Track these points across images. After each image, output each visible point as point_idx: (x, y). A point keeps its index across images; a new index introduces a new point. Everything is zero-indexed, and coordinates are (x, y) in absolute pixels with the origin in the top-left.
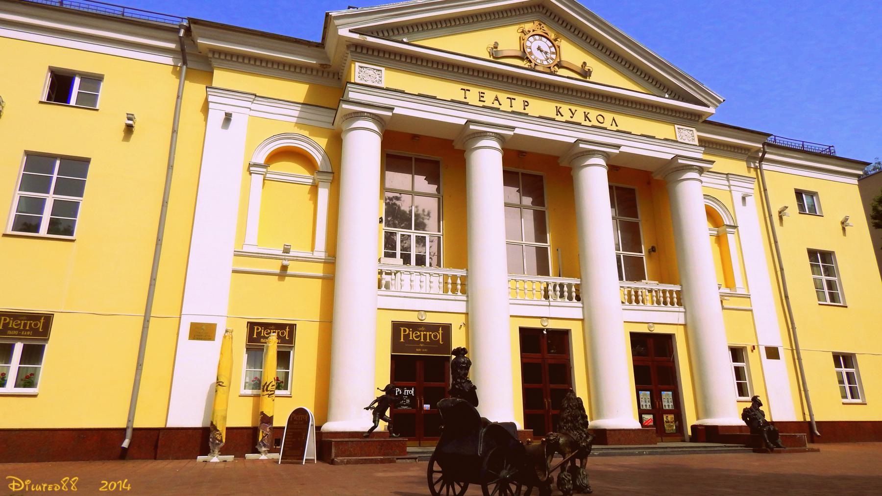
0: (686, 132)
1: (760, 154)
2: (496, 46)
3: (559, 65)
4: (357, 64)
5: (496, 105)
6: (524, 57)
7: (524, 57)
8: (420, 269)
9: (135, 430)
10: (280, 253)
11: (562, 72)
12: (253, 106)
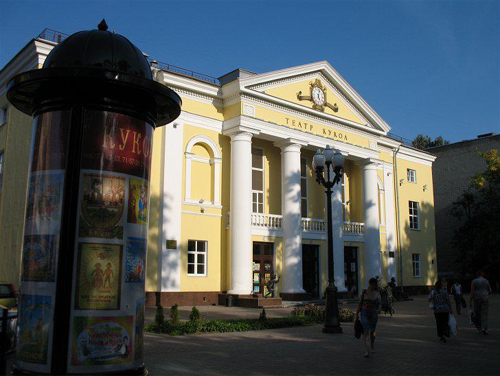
1: (397, 150)
2: (300, 93)
5: (299, 128)
6: (311, 99)
7: (311, 99)
8: (261, 214)
10: (198, 202)
11: (327, 109)
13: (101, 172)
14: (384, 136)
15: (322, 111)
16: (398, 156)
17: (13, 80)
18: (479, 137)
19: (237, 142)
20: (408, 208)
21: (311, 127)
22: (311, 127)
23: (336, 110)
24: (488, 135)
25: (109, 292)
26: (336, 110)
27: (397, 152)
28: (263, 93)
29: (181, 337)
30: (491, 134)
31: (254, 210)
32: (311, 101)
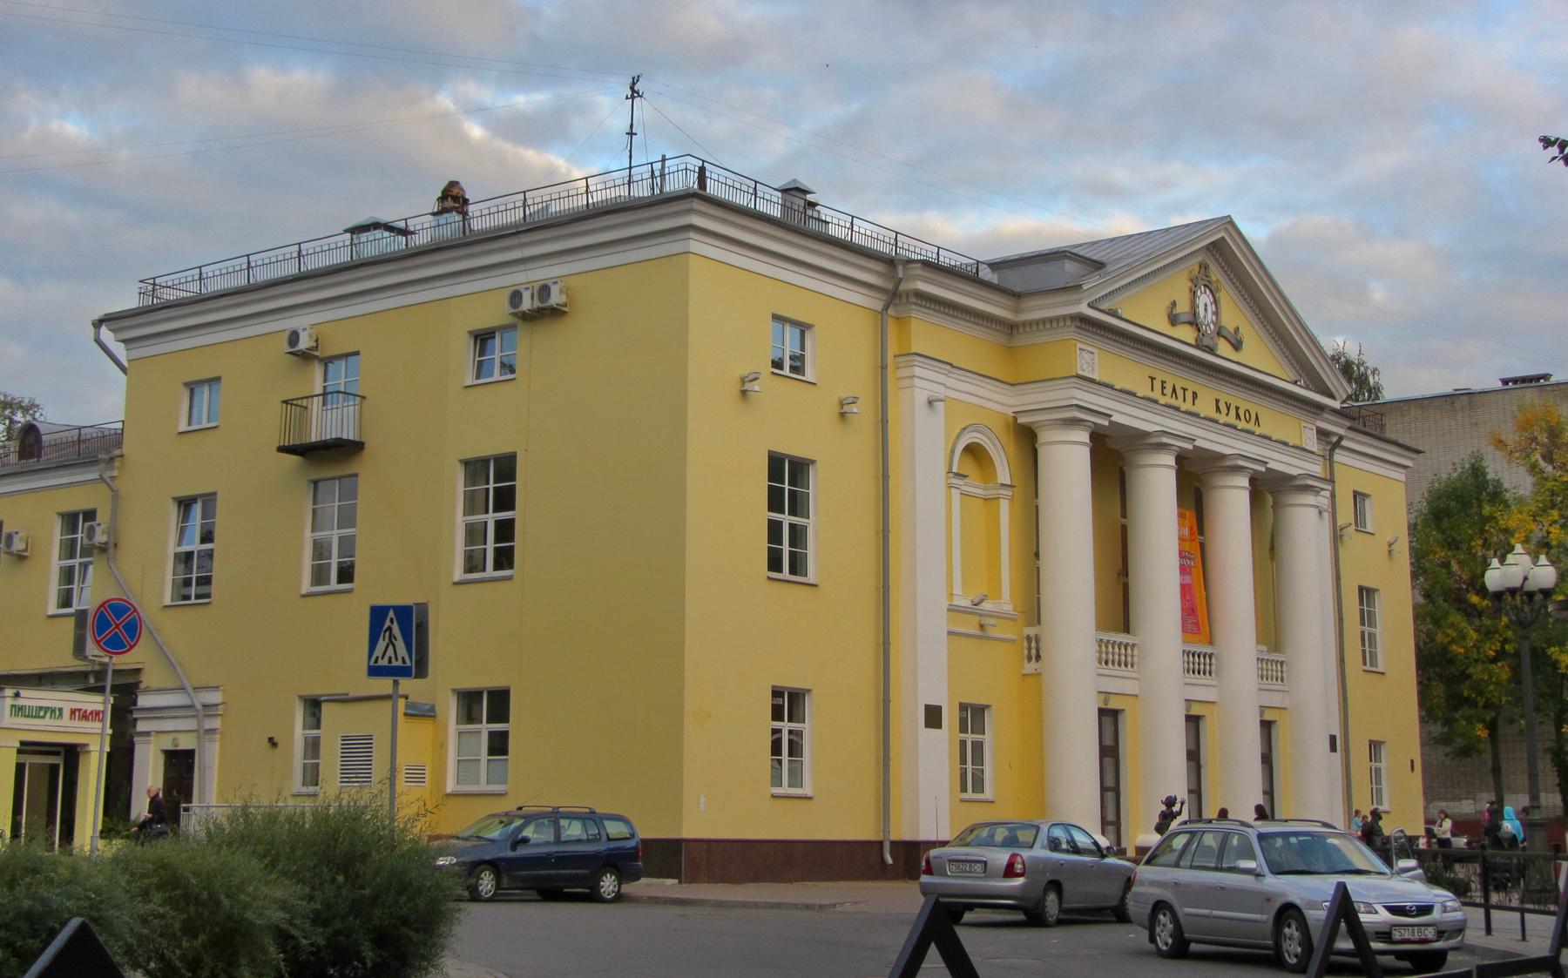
0: (1087, 356)
1: (1335, 439)
2: (1174, 304)
3: (1220, 333)
4: (1079, 345)
5: (1173, 402)
6: (1194, 323)
7: (1194, 323)
9: (893, 843)
12: (951, 382)
13: (492, 486)
14: (1334, 411)
15: (1211, 350)
16: (1339, 456)
17: (933, 950)
18: (1505, 382)
19: (1299, 509)
20: (763, 483)
21: (1195, 395)
22: (1195, 395)
23: (1237, 346)
24: (1537, 378)
25: (390, 629)
26: (1237, 346)
27: (1337, 445)
28: (1113, 314)
29: (539, 274)
30: (1546, 377)
31: (774, 563)
32: (1191, 323)
